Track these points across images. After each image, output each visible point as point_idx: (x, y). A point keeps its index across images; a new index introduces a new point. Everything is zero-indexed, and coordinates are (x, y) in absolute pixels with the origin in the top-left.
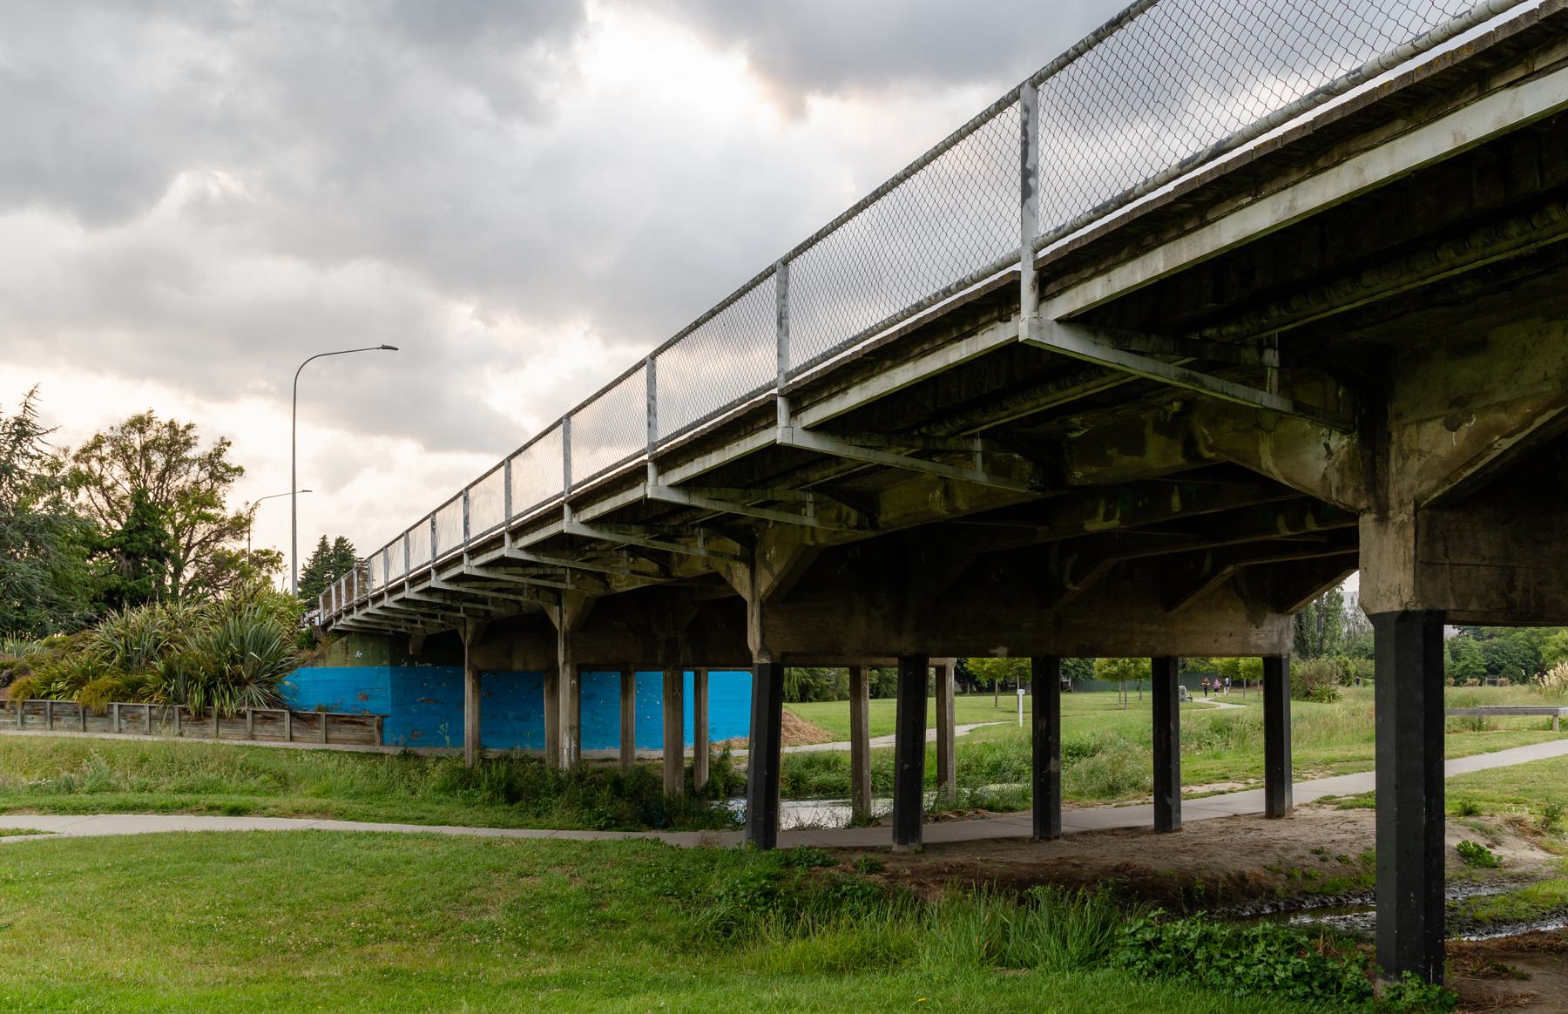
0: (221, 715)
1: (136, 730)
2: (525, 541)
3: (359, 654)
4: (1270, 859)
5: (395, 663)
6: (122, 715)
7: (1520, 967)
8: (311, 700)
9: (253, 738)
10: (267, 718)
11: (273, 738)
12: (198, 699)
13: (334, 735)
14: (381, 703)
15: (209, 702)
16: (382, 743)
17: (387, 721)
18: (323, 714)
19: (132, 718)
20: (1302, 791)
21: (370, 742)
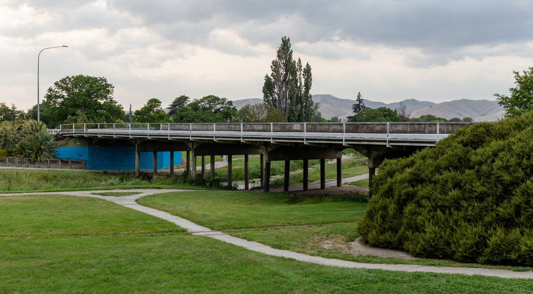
0: (41, 161)
1: (13, 166)
2: (245, 140)
3: (78, 143)
4: (344, 193)
5: (89, 146)
6: (9, 161)
7: (451, 169)
8: (64, 156)
9: (50, 167)
10: (54, 162)
11: (55, 167)
12: (33, 156)
13: (73, 166)
14: (85, 157)
15: (37, 157)
16: (86, 169)
17: (87, 162)
18: (70, 161)
19: (12, 162)
20: (344, 181)
21: (83, 168)
